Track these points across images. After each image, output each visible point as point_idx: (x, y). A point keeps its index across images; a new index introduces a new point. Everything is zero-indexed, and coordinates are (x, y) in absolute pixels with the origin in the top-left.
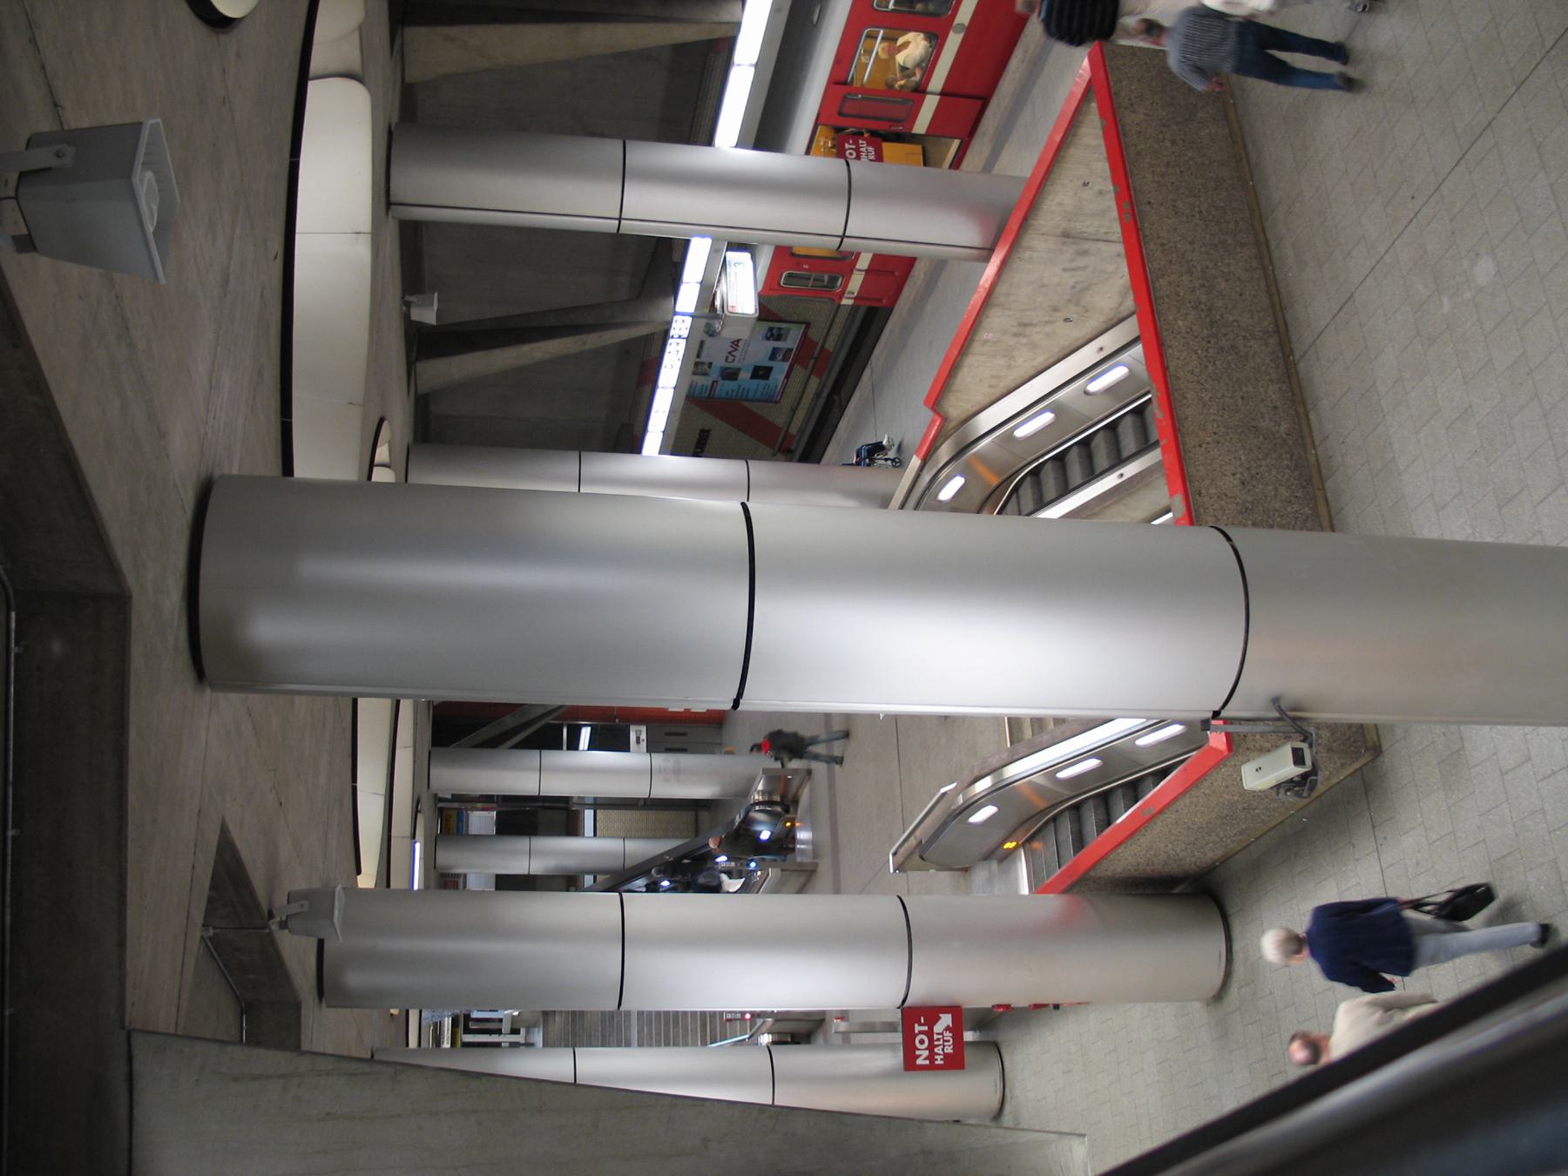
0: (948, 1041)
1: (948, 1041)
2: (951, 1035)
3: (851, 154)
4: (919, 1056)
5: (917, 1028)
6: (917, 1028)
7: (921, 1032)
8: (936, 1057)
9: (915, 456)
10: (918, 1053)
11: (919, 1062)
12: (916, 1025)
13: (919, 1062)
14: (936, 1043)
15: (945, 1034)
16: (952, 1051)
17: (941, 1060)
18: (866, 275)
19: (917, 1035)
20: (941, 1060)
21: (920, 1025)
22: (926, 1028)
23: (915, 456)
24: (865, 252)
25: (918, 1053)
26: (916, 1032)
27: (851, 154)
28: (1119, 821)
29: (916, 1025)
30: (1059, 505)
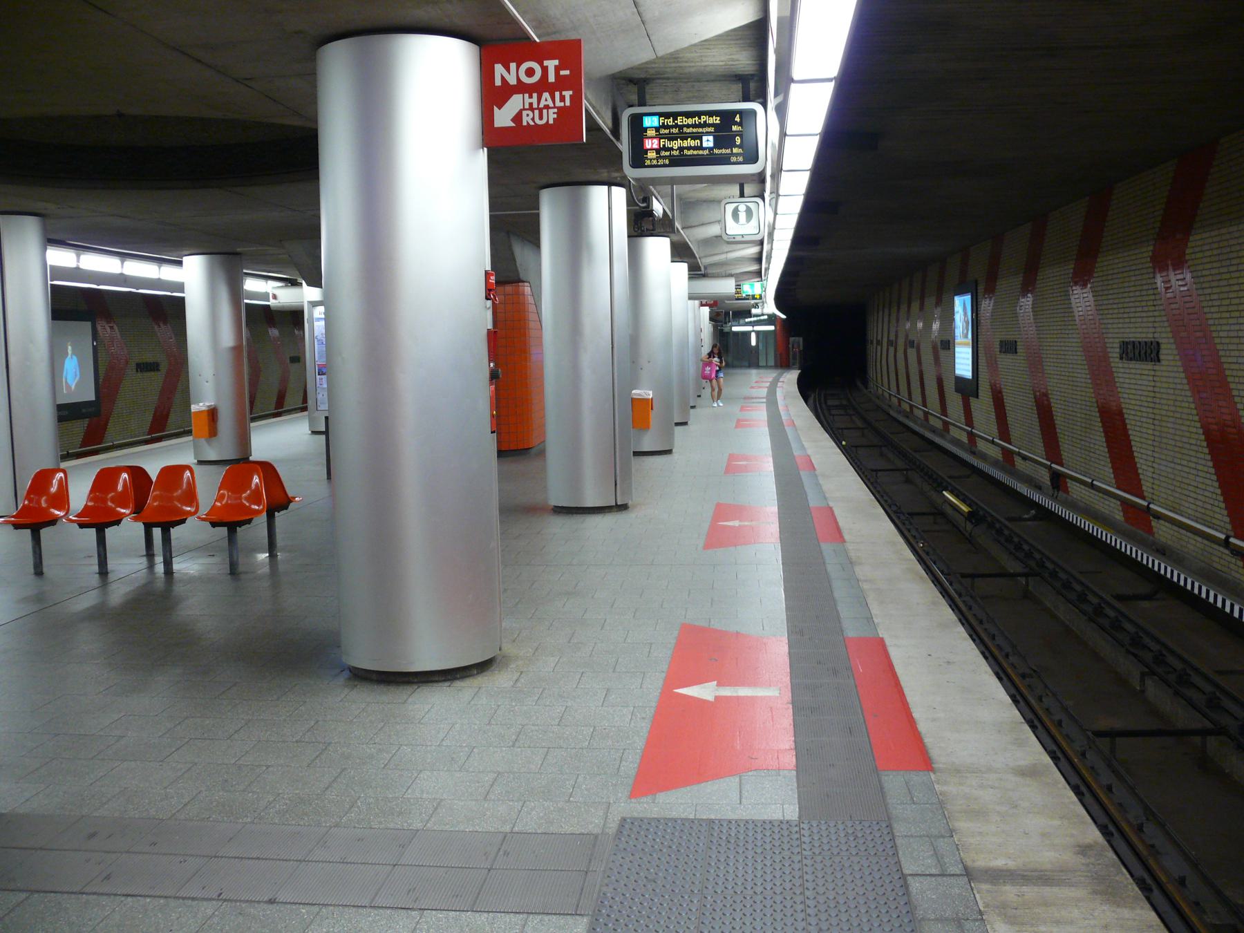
0: (541, 118)
1: (541, 118)
2: (551, 122)
3: (530, 72)
4: (508, 70)
5: (551, 64)
6: (551, 64)
7: (545, 70)
8: (535, 95)
9: (716, 682)
10: (513, 66)
11: (499, 69)
12: (556, 62)
13: (499, 69)
14: (557, 94)
15: (551, 111)
16: (525, 123)
17: (531, 97)
18: (656, 185)
19: (541, 64)
20: (531, 97)
21: (557, 69)
22: (552, 78)
23: (716, 682)
24: (762, 286)
25: (513, 66)
26: (546, 63)
27: (530, 72)
28: (70, 348)
29: (556, 62)
30: (55, 251)
